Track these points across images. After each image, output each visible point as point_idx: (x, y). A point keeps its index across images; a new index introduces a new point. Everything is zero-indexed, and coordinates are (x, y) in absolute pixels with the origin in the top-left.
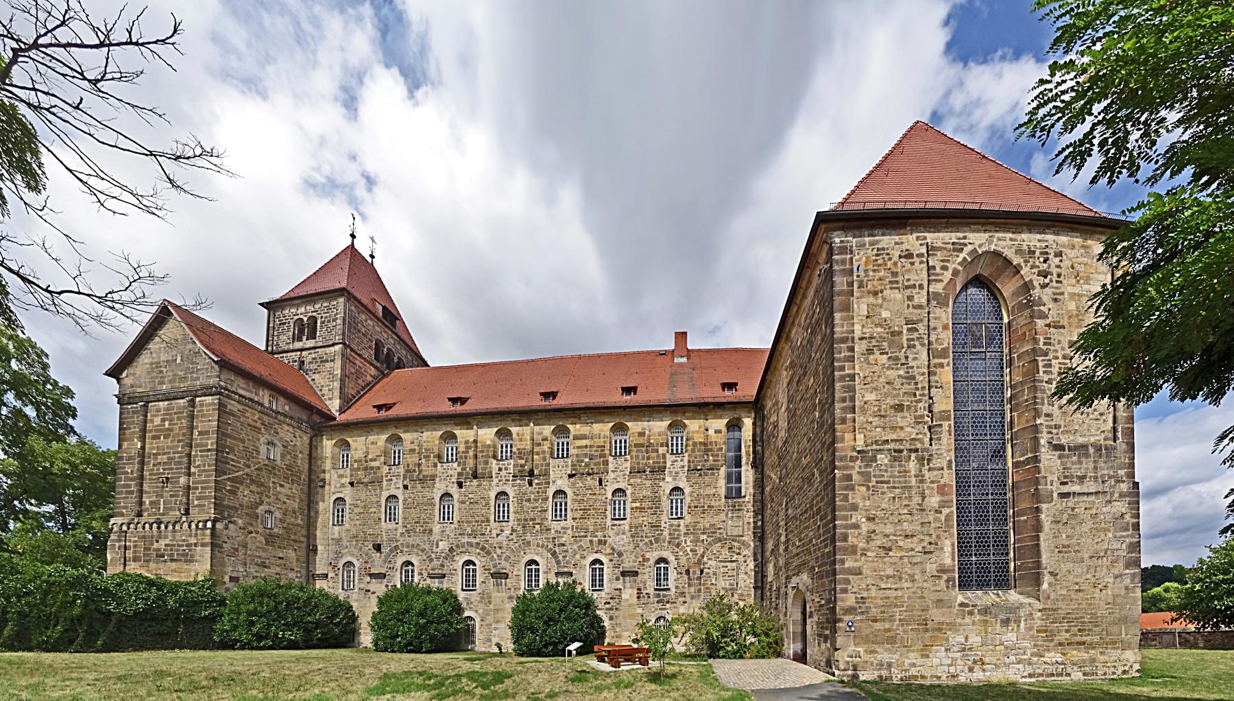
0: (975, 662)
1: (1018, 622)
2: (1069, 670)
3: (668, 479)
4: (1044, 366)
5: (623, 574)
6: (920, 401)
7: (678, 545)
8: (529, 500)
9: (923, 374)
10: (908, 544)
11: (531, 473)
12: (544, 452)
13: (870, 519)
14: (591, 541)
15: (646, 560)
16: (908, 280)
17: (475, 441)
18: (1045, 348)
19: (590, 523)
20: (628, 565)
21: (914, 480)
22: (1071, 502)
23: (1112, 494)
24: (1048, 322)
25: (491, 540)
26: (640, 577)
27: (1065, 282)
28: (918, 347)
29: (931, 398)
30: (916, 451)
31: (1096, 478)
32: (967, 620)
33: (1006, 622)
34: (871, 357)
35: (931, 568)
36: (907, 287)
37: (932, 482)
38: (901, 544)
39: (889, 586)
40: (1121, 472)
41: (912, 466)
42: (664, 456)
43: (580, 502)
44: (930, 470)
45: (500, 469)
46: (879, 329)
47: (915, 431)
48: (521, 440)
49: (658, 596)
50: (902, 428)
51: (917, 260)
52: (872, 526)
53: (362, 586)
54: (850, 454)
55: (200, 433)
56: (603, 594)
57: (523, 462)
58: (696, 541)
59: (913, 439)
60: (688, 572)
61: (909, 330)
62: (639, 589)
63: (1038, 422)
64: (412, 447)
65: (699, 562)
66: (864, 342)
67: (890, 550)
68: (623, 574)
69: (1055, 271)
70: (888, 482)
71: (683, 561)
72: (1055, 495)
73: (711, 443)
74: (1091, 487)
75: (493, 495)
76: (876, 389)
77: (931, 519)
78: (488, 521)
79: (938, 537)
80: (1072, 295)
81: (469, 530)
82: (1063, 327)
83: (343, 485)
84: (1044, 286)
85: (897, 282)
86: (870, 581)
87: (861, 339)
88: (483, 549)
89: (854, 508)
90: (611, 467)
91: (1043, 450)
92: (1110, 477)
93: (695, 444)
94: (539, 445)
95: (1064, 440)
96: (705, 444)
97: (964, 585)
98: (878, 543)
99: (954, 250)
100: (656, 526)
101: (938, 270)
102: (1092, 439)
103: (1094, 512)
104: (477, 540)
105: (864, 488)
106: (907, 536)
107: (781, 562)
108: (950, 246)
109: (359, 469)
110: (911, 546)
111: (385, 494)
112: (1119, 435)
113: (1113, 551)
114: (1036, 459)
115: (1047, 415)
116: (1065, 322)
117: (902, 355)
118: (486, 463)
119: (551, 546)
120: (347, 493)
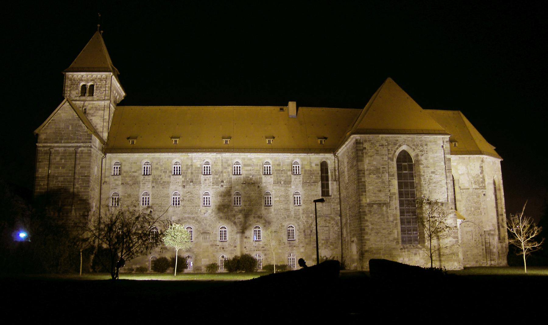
3: (293, 187)
7: (299, 219)
12: (228, 172)
13: (372, 224)
15: (282, 226)
17: (192, 165)
25: (201, 216)
42: (290, 176)
45: (205, 180)
48: (216, 165)
49: (290, 243)
55: (81, 167)
56: (261, 243)
57: (217, 176)
64: (157, 166)
71: (302, 226)
73: (313, 170)
78: (199, 206)
83: (117, 185)
88: (197, 220)
89: (367, 221)
93: (305, 171)
94: (226, 168)
107: (348, 231)
118: (198, 176)
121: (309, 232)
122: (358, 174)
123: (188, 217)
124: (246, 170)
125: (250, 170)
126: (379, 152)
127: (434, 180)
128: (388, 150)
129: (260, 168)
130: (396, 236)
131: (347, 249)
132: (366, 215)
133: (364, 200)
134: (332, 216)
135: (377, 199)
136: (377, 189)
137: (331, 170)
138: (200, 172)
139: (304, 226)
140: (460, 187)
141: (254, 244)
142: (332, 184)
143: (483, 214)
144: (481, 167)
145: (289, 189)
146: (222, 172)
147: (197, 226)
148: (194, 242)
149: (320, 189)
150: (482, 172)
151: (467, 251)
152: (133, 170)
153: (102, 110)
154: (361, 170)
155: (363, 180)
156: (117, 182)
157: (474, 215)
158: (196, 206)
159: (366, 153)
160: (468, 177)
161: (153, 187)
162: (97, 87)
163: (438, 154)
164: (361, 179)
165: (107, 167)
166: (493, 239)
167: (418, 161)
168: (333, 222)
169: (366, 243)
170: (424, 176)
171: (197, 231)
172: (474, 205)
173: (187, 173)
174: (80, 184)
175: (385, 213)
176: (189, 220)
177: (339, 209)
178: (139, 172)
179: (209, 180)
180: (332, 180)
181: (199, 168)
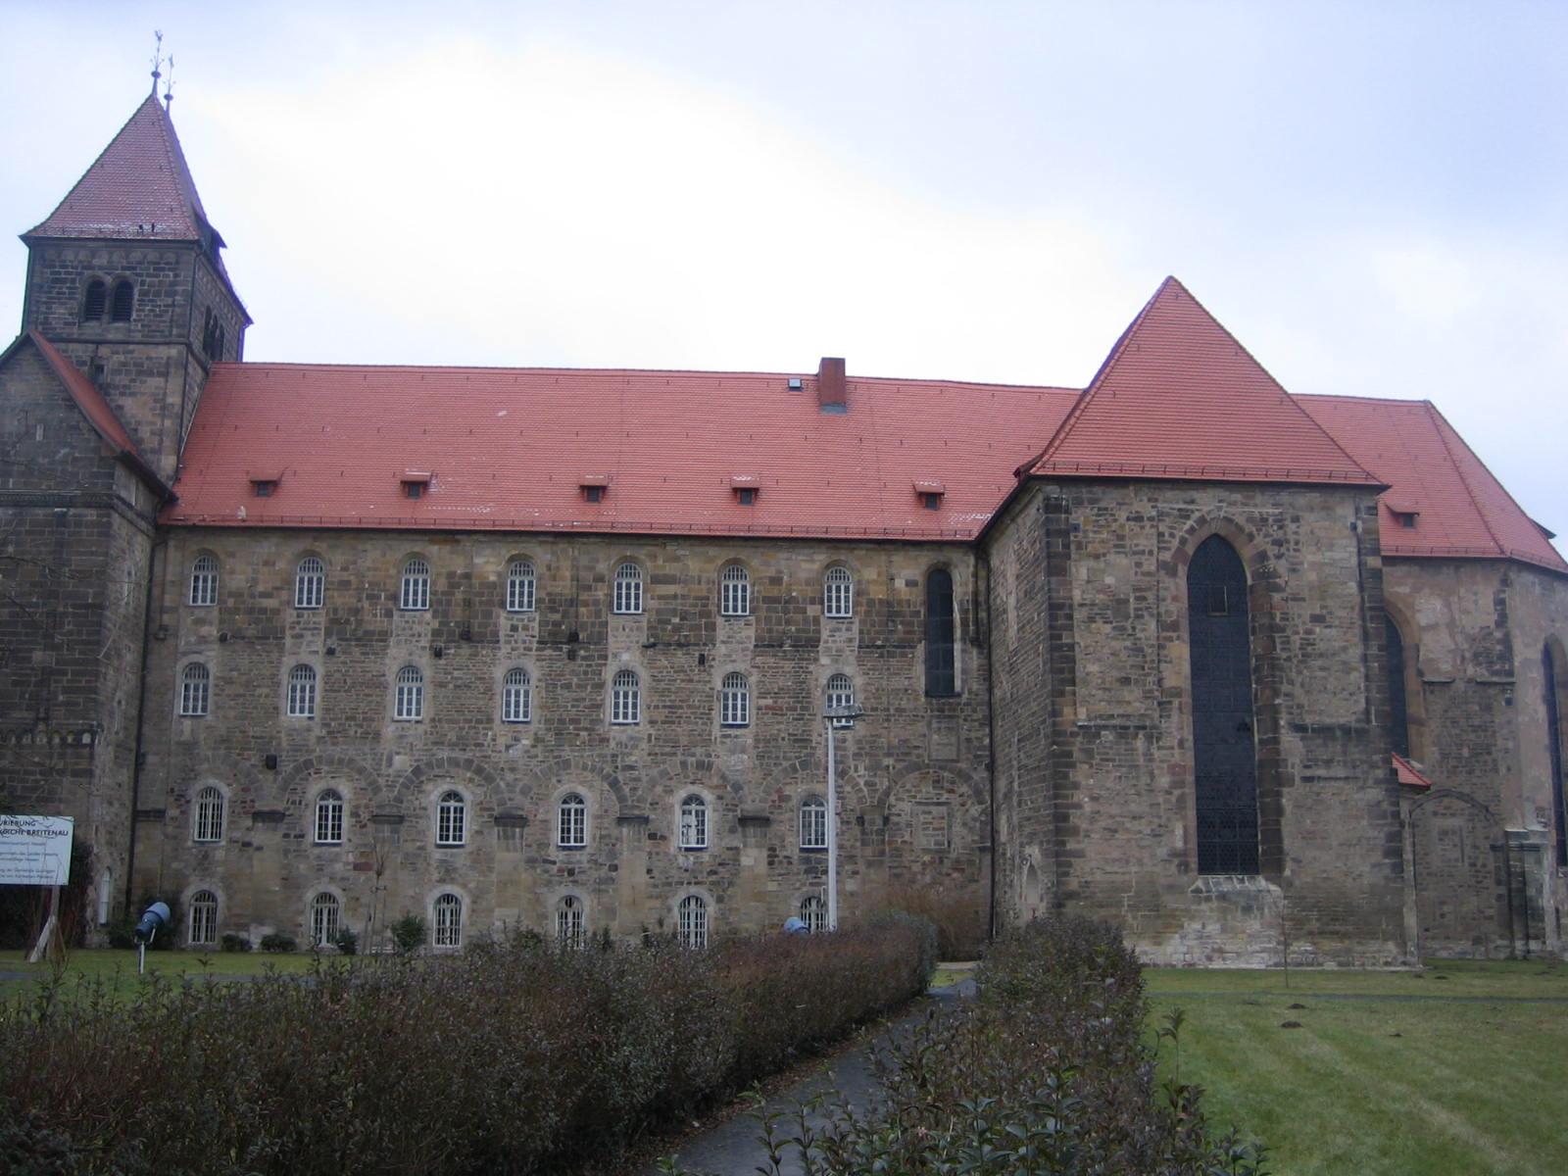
0: (1213, 950)
1: (1261, 909)
2: (1321, 960)
3: (824, 660)
4: (1282, 643)
5: (744, 821)
6: (1149, 674)
8: (568, 686)
9: (1152, 646)
10: (1135, 826)
11: (573, 638)
12: (596, 602)
14: (684, 764)
16: (1137, 545)
18: (1283, 623)
19: (681, 732)
20: (752, 804)
21: (1142, 759)
22: (1316, 786)
23: (1365, 780)
24: (1285, 595)
25: (495, 758)
26: (775, 827)
27: (1304, 549)
28: (1147, 617)
29: (1160, 672)
30: (1144, 728)
31: (1345, 763)
32: (1204, 906)
33: (1247, 909)
34: (1093, 625)
35: (1162, 852)
36: (1135, 553)
37: (1161, 761)
38: (1128, 825)
39: (1115, 869)
40: (1376, 758)
41: (1140, 743)
42: (816, 620)
43: (662, 693)
44: (1159, 748)
45: (514, 628)
46: (1101, 596)
47: (1144, 706)
48: (554, 578)
50: (1129, 703)
51: (1148, 524)
52: (1097, 807)
53: (237, 835)
54: (1069, 730)
56: (706, 857)
57: (557, 617)
58: (874, 768)
59: (1142, 715)
60: (861, 820)
61: (1137, 599)
62: (772, 849)
63: (1277, 701)
64: (345, 576)
65: (881, 803)
66: (1085, 609)
67: (1116, 831)
68: (744, 821)
69: (1292, 538)
70: (1114, 760)
72: (1297, 779)
73: (900, 602)
74: (1341, 772)
75: (499, 673)
76: (1099, 660)
77: (1161, 800)
78: (490, 720)
79: (1169, 819)
80: (1313, 564)
81: (452, 736)
82: (1303, 600)
84: (1279, 557)
85: (1123, 546)
86: (1094, 864)
87: (1081, 605)
88: (479, 771)
90: (721, 633)
91: (1283, 731)
92: (1362, 762)
93: (871, 603)
94: (589, 588)
95: (1309, 720)
96: (889, 604)
97: (1205, 868)
98: (1103, 824)
99: (1181, 517)
100: (802, 741)
101: (1167, 537)
102: (1342, 721)
103: (1344, 798)
104: (468, 755)
105: (1087, 767)
106: (1134, 818)
107: (1015, 820)
108: (1176, 512)
109: (236, 611)
110: (1138, 828)
111: (289, 662)
112: (1373, 717)
113: (1369, 839)
114: (1276, 741)
115: (1286, 695)
116: (1305, 594)
117: (1128, 625)
118: (488, 615)
119: (608, 769)
120: (212, 658)
121: (879, 821)
122: (1052, 617)
123: (450, 759)
124: (660, 597)
125: (675, 597)
126: (1127, 542)
127: (1321, 646)
128: (1161, 535)
129: (709, 591)
130: (1179, 844)
131: (1011, 886)
132: (1072, 765)
133: (1067, 710)
134: (963, 765)
135: (1117, 711)
136: (1115, 674)
137: (961, 604)
138: (496, 599)
139: (860, 800)
140: (1420, 673)
141: (681, 860)
142: (963, 651)
143: (1503, 770)
144: (1500, 603)
145: (811, 668)
146: (573, 602)
147: (478, 791)
148: (469, 849)
149: (919, 671)
150: (1502, 621)
151: (1442, 903)
152: (261, 588)
153: (160, 374)
154: (1061, 606)
155: (1065, 641)
156: (205, 630)
157: (1470, 772)
158: (479, 721)
159: (1079, 546)
160: (1452, 635)
161: (331, 652)
162: (143, 294)
163: (1337, 555)
164: (1060, 637)
165: (169, 578)
166: (1539, 862)
167: (1267, 577)
168: (964, 789)
169: (1070, 865)
170: (1283, 630)
171: (482, 807)
172: (1472, 736)
173: (449, 602)
174: (70, 633)
175: (1141, 761)
176: (453, 771)
177: (987, 741)
178: (284, 595)
179: (525, 628)
180: (963, 640)
181: (494, 585)
